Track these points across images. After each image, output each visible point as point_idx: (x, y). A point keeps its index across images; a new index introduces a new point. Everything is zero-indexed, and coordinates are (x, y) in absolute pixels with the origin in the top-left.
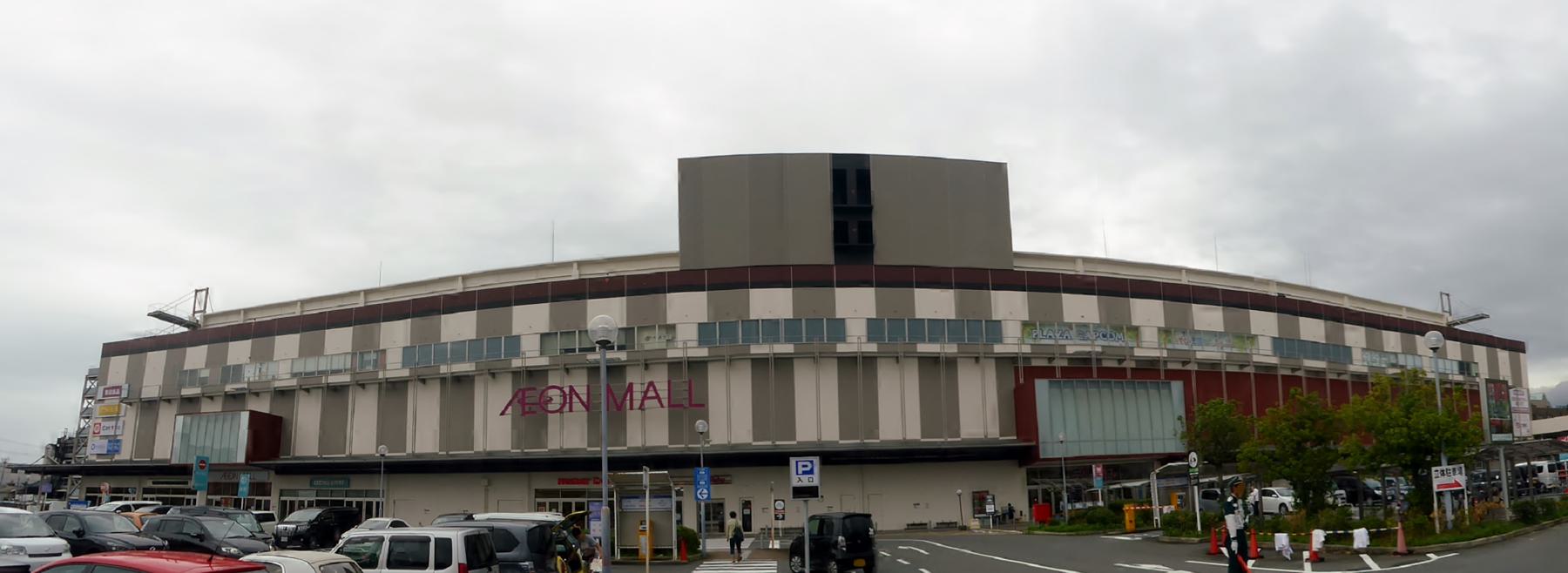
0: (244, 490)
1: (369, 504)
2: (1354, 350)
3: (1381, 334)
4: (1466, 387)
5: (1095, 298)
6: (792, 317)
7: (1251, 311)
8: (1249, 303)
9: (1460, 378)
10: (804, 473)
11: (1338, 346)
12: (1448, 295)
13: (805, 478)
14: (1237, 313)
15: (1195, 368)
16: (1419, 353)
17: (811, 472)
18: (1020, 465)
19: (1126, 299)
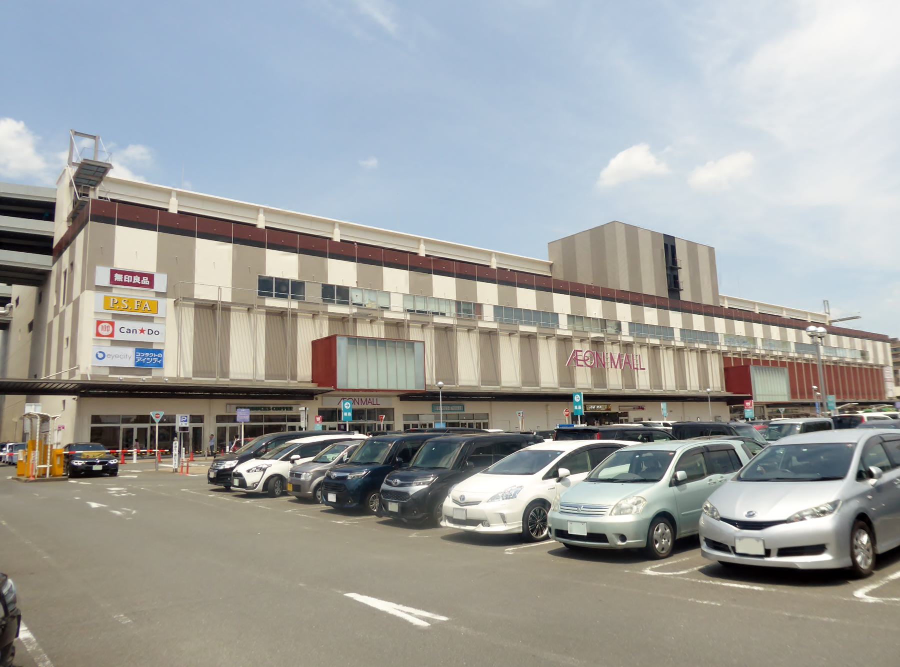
0: (347, 414)
1: (129, 432)
2: (485, 308)
3: (752, 325)
4: (729, 355)
5: (724, 319)
6: (230, 301)
7: (715, 318)
8: (734, 316)
9: (860, 361)
10: (183, 421)
11: (690, 330)
12: (827, 301)
13: (184, 423)
14: (422, 277)
15: (832, 364)
16: (844, 347)
17: (186, 421)
18: (728, 405)
19: (514, 287)
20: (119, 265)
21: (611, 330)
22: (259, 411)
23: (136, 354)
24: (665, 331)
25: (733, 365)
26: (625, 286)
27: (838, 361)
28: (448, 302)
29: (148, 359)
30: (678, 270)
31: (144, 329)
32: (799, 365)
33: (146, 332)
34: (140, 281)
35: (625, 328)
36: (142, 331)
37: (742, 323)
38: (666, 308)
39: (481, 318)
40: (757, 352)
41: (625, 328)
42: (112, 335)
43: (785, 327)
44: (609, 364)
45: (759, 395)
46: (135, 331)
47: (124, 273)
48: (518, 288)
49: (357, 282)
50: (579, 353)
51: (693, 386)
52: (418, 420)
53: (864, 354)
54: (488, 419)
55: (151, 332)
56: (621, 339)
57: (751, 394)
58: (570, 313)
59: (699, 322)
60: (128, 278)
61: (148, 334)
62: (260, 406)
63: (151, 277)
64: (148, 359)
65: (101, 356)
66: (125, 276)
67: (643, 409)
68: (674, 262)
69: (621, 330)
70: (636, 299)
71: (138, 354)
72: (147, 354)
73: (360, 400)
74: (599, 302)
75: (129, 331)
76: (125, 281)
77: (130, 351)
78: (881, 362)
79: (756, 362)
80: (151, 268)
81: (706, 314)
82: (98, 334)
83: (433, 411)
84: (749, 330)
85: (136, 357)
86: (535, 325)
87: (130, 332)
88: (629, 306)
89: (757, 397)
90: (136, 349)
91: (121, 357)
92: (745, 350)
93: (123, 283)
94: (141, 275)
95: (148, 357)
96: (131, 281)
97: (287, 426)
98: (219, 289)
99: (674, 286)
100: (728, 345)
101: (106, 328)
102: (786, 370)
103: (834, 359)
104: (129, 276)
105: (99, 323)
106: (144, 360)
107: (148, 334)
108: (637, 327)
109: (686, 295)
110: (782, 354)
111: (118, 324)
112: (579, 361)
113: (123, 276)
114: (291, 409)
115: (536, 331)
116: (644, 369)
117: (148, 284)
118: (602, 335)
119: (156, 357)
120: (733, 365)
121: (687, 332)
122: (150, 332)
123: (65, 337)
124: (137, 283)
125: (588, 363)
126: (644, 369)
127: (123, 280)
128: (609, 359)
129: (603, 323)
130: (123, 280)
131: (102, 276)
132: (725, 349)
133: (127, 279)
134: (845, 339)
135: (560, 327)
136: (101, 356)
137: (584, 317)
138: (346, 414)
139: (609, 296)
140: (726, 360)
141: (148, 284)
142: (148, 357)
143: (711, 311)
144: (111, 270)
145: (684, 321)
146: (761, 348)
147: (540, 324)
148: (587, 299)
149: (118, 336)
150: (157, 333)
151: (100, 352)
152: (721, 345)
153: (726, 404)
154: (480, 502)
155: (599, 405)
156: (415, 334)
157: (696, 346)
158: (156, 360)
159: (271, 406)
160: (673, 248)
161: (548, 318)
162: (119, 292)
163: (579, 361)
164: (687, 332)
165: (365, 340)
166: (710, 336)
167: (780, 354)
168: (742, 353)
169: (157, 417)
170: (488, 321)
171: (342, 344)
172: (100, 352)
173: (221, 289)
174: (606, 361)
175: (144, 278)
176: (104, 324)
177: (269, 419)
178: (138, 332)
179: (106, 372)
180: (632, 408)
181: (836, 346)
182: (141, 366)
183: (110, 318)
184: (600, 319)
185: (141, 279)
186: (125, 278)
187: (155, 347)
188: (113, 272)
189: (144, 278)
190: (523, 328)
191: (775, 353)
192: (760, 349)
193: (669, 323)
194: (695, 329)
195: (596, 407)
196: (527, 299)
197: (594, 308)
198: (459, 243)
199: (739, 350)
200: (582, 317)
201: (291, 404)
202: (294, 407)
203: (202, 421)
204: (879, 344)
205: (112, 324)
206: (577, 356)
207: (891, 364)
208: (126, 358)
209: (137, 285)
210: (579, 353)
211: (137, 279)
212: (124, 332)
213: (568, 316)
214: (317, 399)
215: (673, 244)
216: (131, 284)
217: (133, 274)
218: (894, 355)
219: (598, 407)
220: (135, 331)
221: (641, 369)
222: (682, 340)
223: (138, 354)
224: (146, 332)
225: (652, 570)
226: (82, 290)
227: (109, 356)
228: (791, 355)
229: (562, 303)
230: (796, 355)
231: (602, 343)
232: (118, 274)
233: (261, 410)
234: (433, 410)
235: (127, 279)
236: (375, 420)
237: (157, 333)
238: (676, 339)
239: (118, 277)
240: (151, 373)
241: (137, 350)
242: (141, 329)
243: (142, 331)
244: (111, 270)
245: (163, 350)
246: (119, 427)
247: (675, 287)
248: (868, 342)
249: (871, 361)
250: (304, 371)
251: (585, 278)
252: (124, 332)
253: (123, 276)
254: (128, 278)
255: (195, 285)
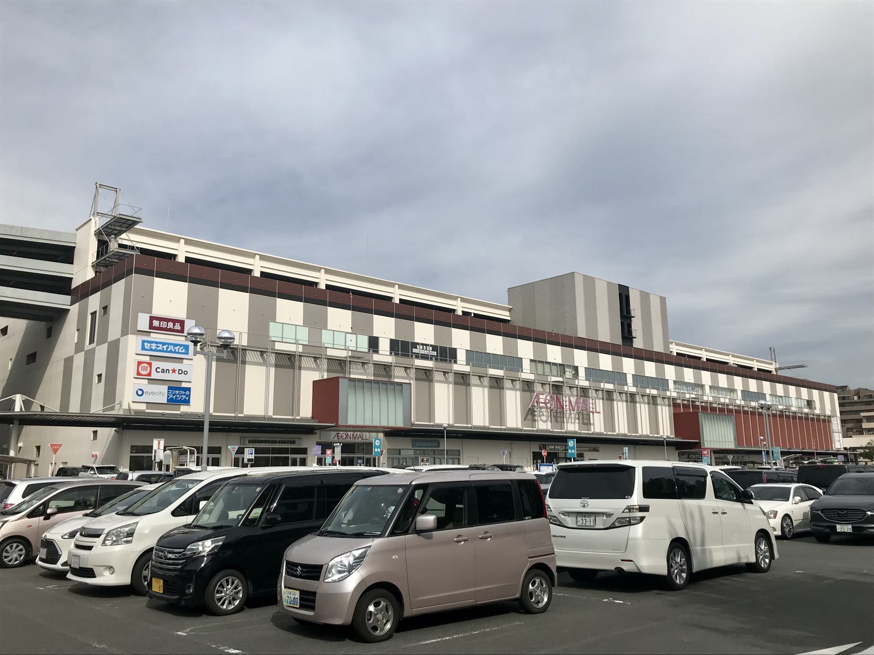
3: (664, 366)
4: (679, 401)
9: (806, 410)
17: (252, 454)
20: (156, 312)
21: (569, 374)
22: (268, 444)
23: (168, 392)
24: (618, 377)
25: (682, 411)
26: (582, 333)
27: (348, 359)
28: (563, 367)
29: (178, 396)
30: (632, 319)
31: (175, 369)
32: (746, 412)
33: (177, 372)
34: (173, 327)
35: (582, 373)
36: (174, 371)
37: (653, 364)
38: (620, 355)
39: (455, 362)
40: (705, 398)
41: (582, 373)
42: (149, 374)
43: (799, 386)
44: (568, 407)
45: (707, 441)
46: (168, 371)
47: (160, 319)
48: (220, 290)
49: (351, 328)
50: (541, 396)
51: (644, 430)
52: (400, 454)
53: (810, 403)
54: (459, 455)
55: (181, 372)
56: (551, 380)
57: (700, 440)
58: (742, 389)
59: (650, 369)
60: (164, 324)
61: (179, 374)
62: (268, 439)
63: (182, 323)
64: (178, 396)
65: (140, 393)
66: (161, 322)
67: (597, 451)
68: (628, 311)
69: (578, 375)
70: (593, 346)
71: (170, 392)
72: (177, 392)
73: (352, 435)
74: (530, 344)
75: (163, 371)
76: (161, 326)
77: (164, 389)
78: (828, 413)
79: (704, 409)
80: (181, 314)
81: (657, 361)
82: (138, 373)
83: (413, 447)
84: (698, 377)
85: (168, 394)
86: (502, 369)
87: (164, 372)
88: (468, 332)
89: (705, 443)
90: (168, 387)
91: (157, 394)
92: (693, 396)
93: (159, 329)
94: (174, 321)
95: (178, 394)
96: (166, 326)
97: (290, 458)
98: (240, 334)
99: (627, 335)
100: (677, 391)
101: (144, 369)
102: (733, 417)
103: (780, 407)
104: (164, 322)
105: (139, 363)
106: (174, 397)
107: (179, 374)
108: (593, 372)
109: (638, 343)
110: (713, 399)
111: (155, 364)
112: (540, 404)
113: (160, 322)
114: (294, 442)
115: (469, 371)
116: (599, 413)
117: (180, 329)
118: (561, 379)
119: (184, 394)
120: (682, 411)
121: (640, 379)
122: (180, 372)
123: (96, 372)
124: (171, 328)
125: (549, 405)
126: (599, 413)
127: (160, 325)
128: (567, 403)
129: (562, 366)
130: (160, 325)
131: (143, 322)
132: (674, 395)
133: (162, 325)
134: (792, 389)
135: (458, 362)
136: (140, 393)
137: (545, 362)
138: (376, 450)
139: (569, 342)
140: (676, 405)
141: (180, 329)
142: (178, 394)
143: (661, 359)
144: (150, 316)
145: (636, 367)
146: (709, 395)
147: (506, 368)
148: (518, 340)
149: (154, 375)
150: (186, 373)
151: (140, 390)
152: (671, 392)
153: (675, 449)
154: (613, 514)
155: (558, 445)
156: (399, 375)
157: (648, 391)
158: (184, 397)
159: (278, 440)
160: (627, 297)
161: (513, 362)
162: (156, 337)
163: (540, 404)
164: (640, 379)
165: (354, 380)
166: (661, 383)
167: (727, 401)
168: (691, 400)
169: (233, 451)
170: (461, 365)
171: (343, 384)
172: (140, 390)
173: (241, 334)
174: (564, 404)
175: (176, 324)
176: (143, 365)
177: (274, 451)
178: (171, 372)
179: (143, 407)
180: (587, 449)
181: (782, 395)
182: (173, 401)
183: (147, 359)
184: (559, 364)
185: (174, 325)
186: (161, 324)
187: (184, 385)
188: (152, 319)
189: (176, 324)
190: (493, 372)
191: (722, 400)
192: (708, 396)
193: (644, 372)
194: (646, 375)
195: (555, 447)
196: (494, 344)
197: (554, 353)
198: (368, 275)
199: (687, 396)
200: (543, 362)
201: (295, 438)
202: (297, 441)
203: (220, 453)
204: (826, 394)
205: (150, 364)
206: (539, 399)
207: (838, 414)
208: (160, 394)
209: (170, 330)
210: (541, 396)
211: (171, 325)
212: (159, 372)
213: (531, 360)
214: (316, 434)
215: (627, 294)
216: (166, 329)
217: (168, 320)
218: (841, 405)
219: (556, 447)
220: (168, 371)
221: (596, 412)
222: (586, 380)
223: (170, 392)
224: (177, 372)
225: (676, 579)
226: (125, 333)
227: (147, 392)
228: (738, 402)
229: (525, 349)
230: (743, 403)
231: (561, 387)
232: (156, 320)
233: (269, 443)
234: (413, 444)
235: (162, 325)
236: (364, 454)
237: (186, 373)
238: (629, 385)
239: (156, 323)
240: (180, 409)
241: (169, 388)
242: (173, 369)
243: (174, 371)
244: (150, 316)
245: (190, 388)
246: (288, 457)
247: (629, 335)
248: (815, 393)
249: (817, 411)
250: (305, 410)
251: (544, 325)
252: (159, 372)
253: (160, 322)
254: (164, 324)
255: (247, 332)
